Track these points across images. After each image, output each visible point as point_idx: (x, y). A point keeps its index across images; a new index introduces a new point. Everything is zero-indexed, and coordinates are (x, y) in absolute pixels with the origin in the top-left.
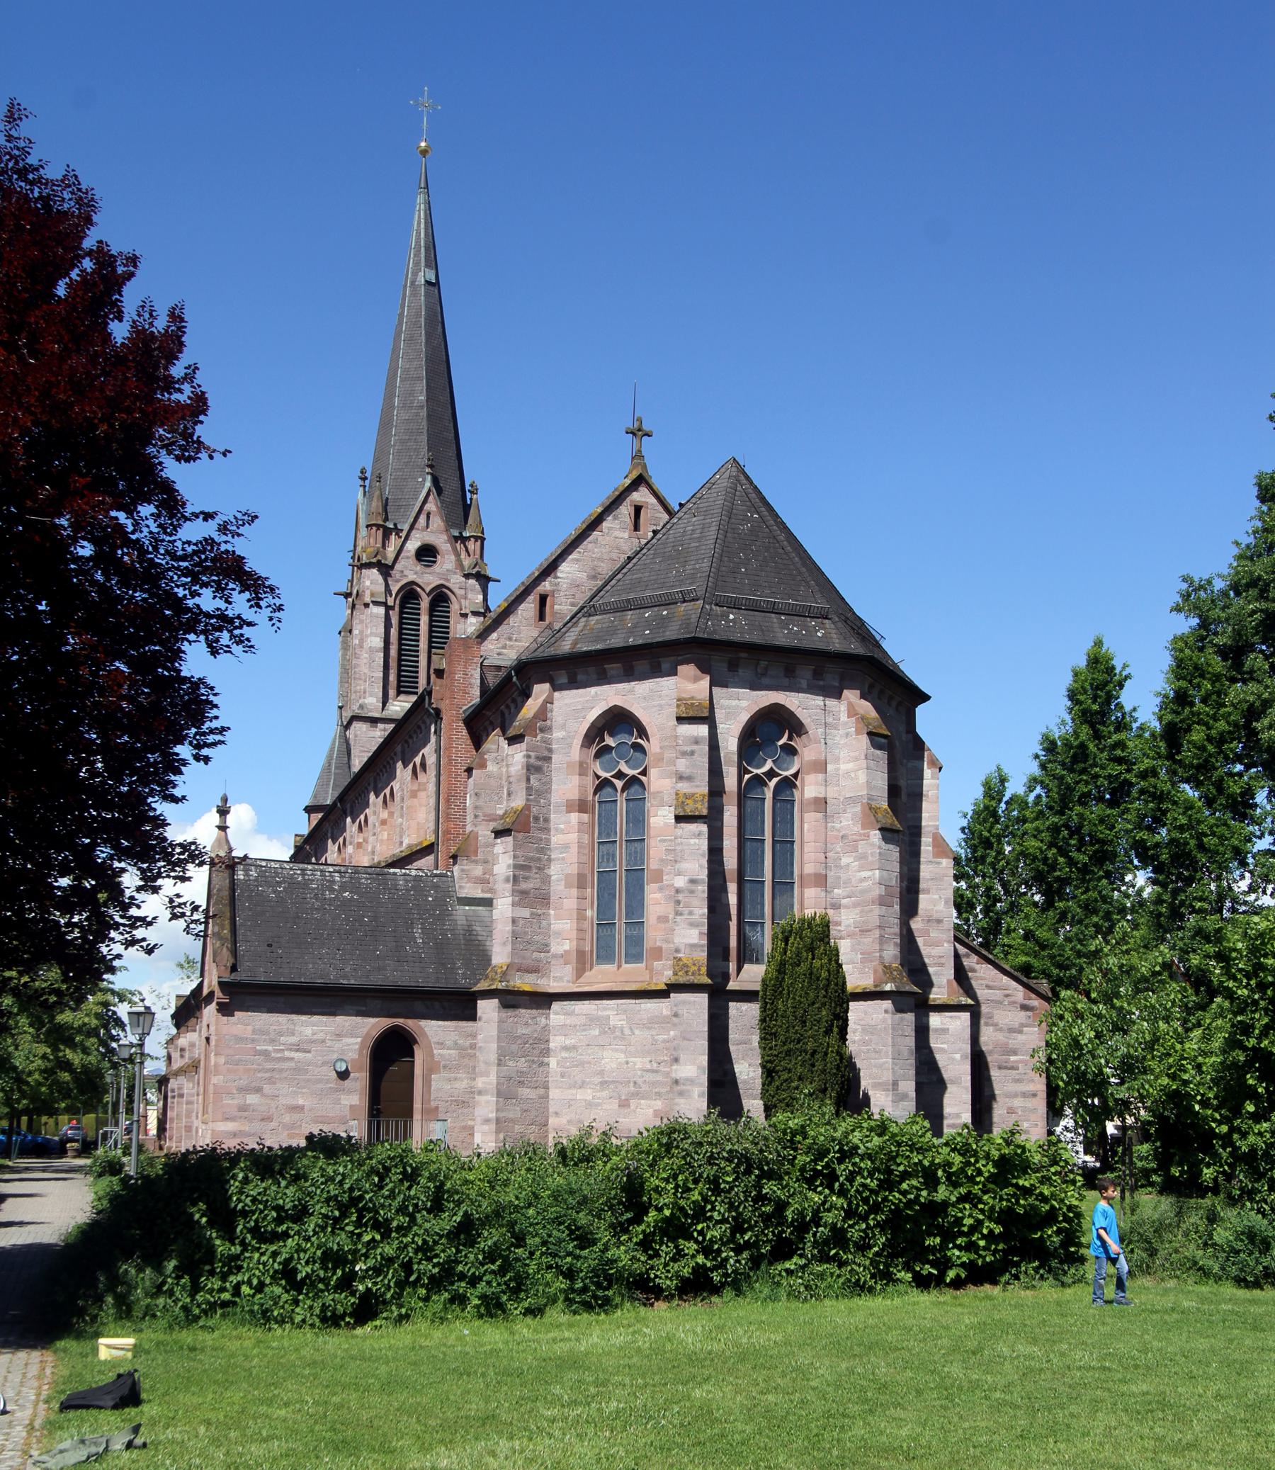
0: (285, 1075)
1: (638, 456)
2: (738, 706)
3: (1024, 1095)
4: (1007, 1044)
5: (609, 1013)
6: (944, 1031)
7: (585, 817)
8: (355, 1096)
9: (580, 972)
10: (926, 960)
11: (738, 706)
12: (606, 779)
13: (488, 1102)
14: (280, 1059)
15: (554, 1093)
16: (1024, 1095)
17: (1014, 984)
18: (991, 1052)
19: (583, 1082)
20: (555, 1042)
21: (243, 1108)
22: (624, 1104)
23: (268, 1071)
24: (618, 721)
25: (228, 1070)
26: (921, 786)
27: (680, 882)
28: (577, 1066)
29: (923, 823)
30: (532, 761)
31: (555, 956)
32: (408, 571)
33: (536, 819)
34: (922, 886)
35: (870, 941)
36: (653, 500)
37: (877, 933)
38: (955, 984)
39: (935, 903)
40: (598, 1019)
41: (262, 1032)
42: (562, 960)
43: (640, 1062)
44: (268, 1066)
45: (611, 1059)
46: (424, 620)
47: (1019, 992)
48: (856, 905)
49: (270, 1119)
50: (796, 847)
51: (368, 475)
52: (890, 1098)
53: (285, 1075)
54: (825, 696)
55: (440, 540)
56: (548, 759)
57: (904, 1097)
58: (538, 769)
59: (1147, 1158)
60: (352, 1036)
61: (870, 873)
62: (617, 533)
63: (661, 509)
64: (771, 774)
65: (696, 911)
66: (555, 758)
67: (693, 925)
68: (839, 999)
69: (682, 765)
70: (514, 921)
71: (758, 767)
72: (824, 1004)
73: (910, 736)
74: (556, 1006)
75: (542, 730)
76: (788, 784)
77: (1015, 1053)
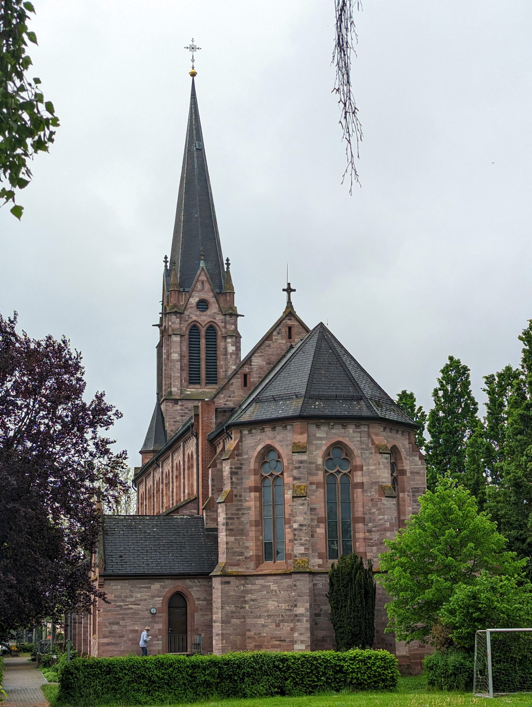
0: (129, 616)
1: (289, 302)
5: (270, 584)
9: (257, 566)
12: (266, 476)
13: (218, 626)
19: (260, 615)
21: (111, 632)
22: (278, 625)
23: (120, 614)
24: (269, 449)
27: (295, 526)
28: (257, 608)
30: (233, 470)
32: (194, 315)
33: (236, 496)
36: (296, 323)
40: (266, 586)
42: (249, 560)
43: (284, 606)
44: (121, 612)
45: (272, 605)
46: (203, 341)
48: (378, 531)
49: (123, 636)
51: (169, 259)
53: (129, 616)
55: (209, 296)
58: (236, 473)
60: (159, 596)
62: (280, 341)
63: (301, 327)
65: (304, 539)
67: (302, 545)
69: (295, 473)
70: (227, 543)
71: (332, 470)
75: (237, 455)
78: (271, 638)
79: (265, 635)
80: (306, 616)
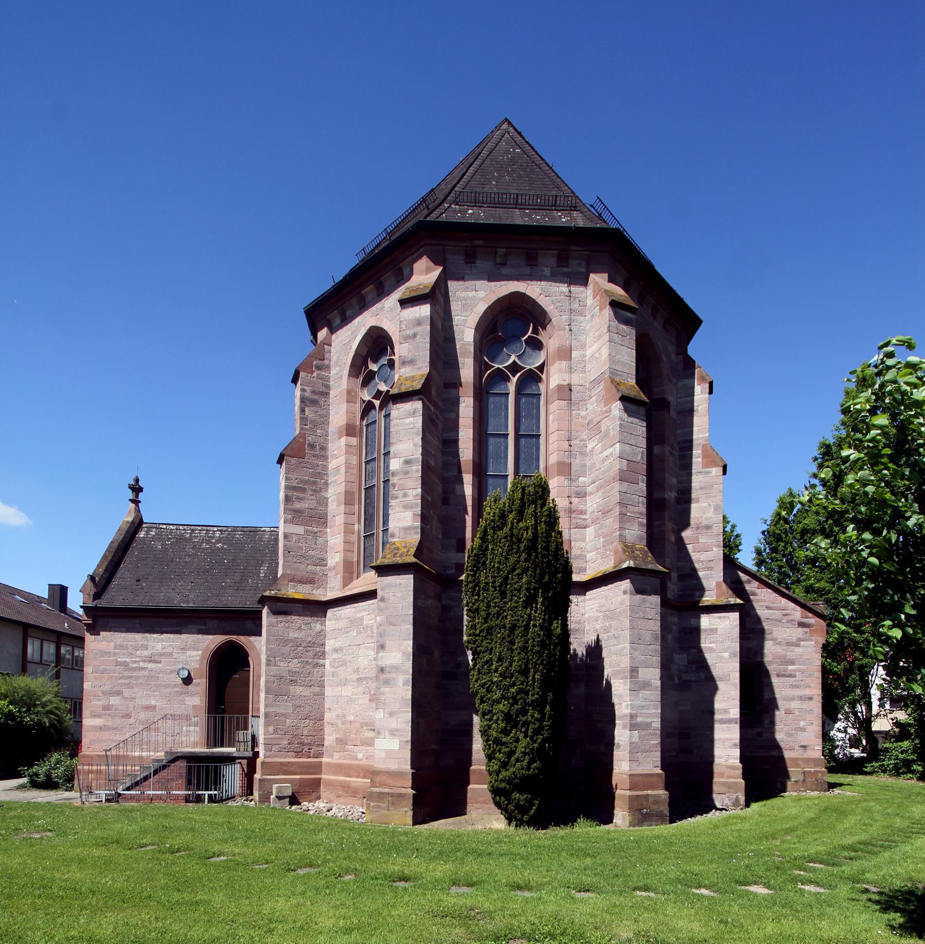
0: (141, 681)
2: (472, 300)
3: (801, 698)
4: (786, 655)
5: (363, 614)
6: (713, 631)
7: (354, 441)
8: (196, 698)
10: (697, 566)
11: (472, 300)
14: (135, 669)
15: (328, 691)
16: (801, 698)
17: (792, 605)
18: (770, 662)
19: (346, 679)
20: (330, 645)
21: (107, 708)
23: (127, 678)
25: (95, 678)
26: (692, 401)
28: (342, 666)
29: (695, 437)
30: (307, 394)
31: (330, 569)
33: (312, 446)
34: (694, 495)
35: (611, 522)
37: (617, 511)
38: (724, 586)
39: (703, 510)
41: (122, 647)
44: (127, 674)
47: (797, 612)
49: (128, 716)
50: (542, 440)
52: (628, 687)
53: (141, 681)
54: (571, 283)
56: (326, 394)
57: (646, 685)
58: (314, 403)
59: (906, 752)
61: (612, 449)
64: (514, 368)
66: (332, 393)
67: (407, 507)
68: (557, 584)
72: (525, 571)
73: (680, 357)
74: (330, 613)
75: (319, 368)
76: (533, 377)
77: (793, 663)
78: (362, 725)
79: (352, 718)
80: (405, 672)
